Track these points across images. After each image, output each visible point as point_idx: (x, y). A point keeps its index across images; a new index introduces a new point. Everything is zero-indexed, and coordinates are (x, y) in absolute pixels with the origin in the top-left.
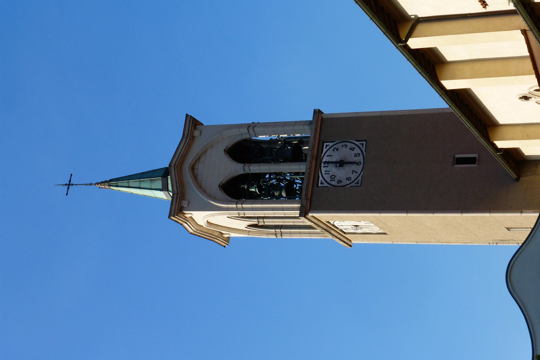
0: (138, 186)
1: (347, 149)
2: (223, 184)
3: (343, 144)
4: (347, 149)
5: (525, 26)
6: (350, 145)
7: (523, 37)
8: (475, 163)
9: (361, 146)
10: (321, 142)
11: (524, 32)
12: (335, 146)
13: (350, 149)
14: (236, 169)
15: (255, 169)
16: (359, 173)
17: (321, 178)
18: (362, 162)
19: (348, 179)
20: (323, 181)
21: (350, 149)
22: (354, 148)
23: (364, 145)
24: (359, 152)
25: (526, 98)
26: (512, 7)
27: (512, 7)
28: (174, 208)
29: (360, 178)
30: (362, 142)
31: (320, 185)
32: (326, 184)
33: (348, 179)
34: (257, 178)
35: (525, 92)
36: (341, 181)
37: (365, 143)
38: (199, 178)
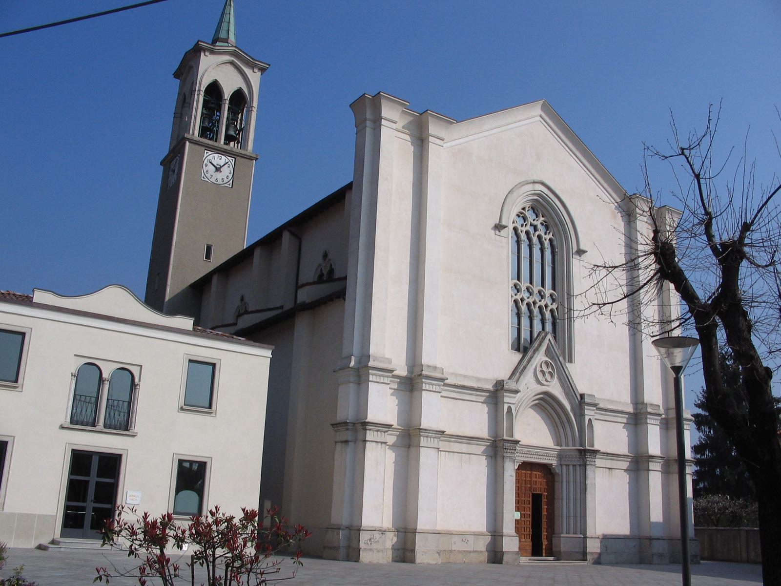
0: (227, 24)
1: (228, 174)
2: (217, 83)
3: (232, 172)
4: (228, 174)
5: (286, 308)
6: (231, 176)
7: (278, 306)
8: (206, 258)
9: (228, 183)
10: (235, 157)
11: (282, 307)
12: (231, 165)
13: (228, 176)
14: (227, 95)
15: (226, 107)
16: (210, 179)
17: (210, 153)
18: (217, 183)
19: (207, 171)
20: (208, 154)
21: (228, 176)
22: (228, 178)
23: (229, 186)
24: (225, 182)
25: (325, 256)
26: (298, 302)
27: (298, 301)
28: (544, 195)
29: (206, 180)
30: (231, 184)
31: (206, 151)
32: (205, 156)
33: (207, 171)
34: (219, 108)
35: (330, 256)
36: (206, 166)
37: (231, 186)
38: (223, 65)
